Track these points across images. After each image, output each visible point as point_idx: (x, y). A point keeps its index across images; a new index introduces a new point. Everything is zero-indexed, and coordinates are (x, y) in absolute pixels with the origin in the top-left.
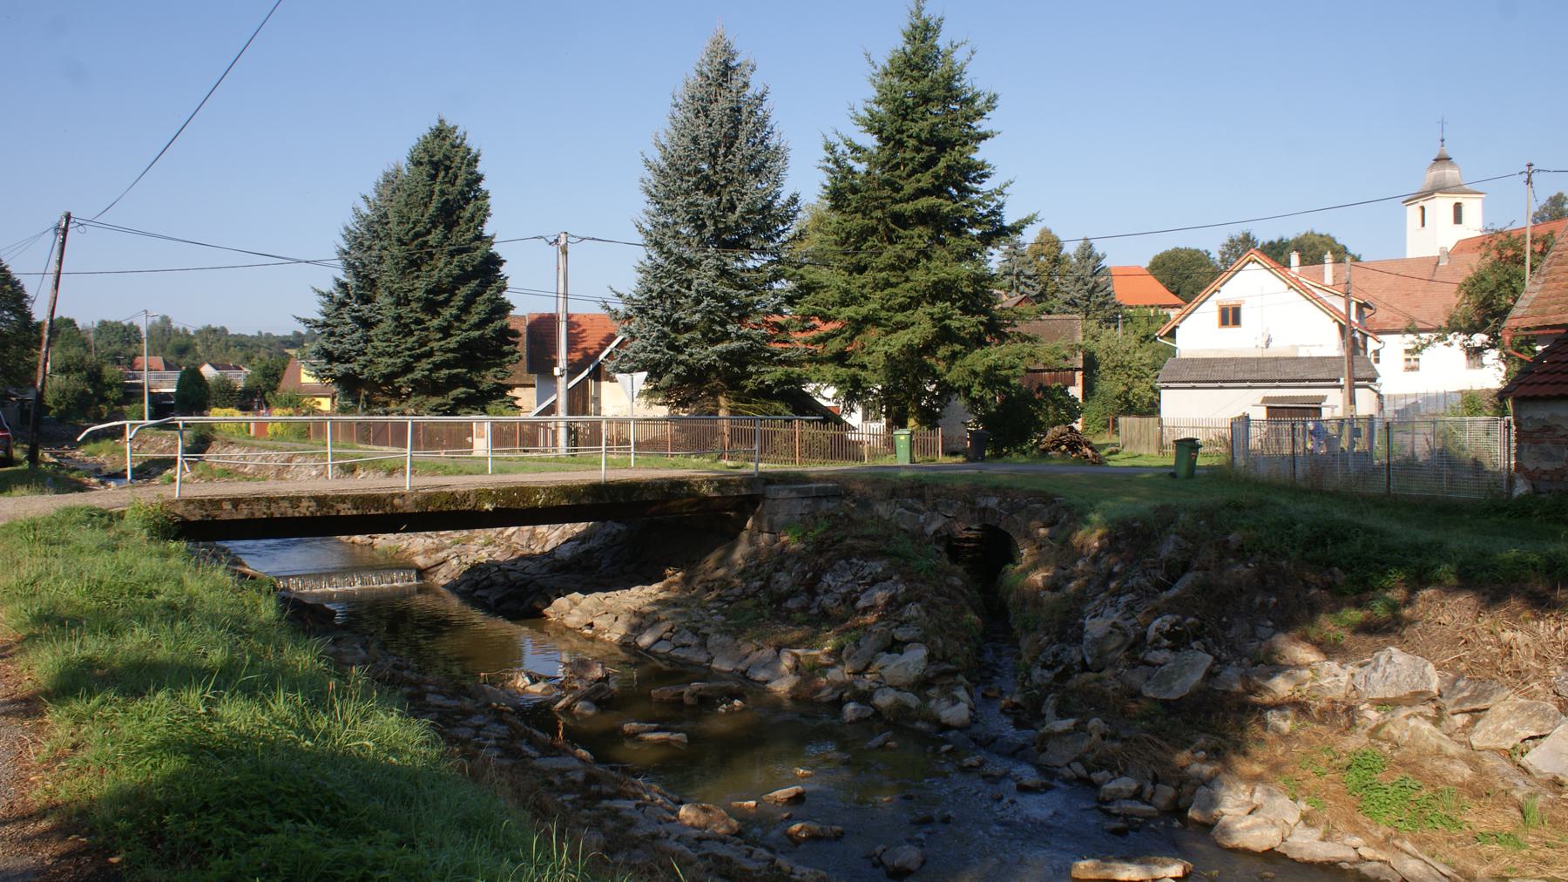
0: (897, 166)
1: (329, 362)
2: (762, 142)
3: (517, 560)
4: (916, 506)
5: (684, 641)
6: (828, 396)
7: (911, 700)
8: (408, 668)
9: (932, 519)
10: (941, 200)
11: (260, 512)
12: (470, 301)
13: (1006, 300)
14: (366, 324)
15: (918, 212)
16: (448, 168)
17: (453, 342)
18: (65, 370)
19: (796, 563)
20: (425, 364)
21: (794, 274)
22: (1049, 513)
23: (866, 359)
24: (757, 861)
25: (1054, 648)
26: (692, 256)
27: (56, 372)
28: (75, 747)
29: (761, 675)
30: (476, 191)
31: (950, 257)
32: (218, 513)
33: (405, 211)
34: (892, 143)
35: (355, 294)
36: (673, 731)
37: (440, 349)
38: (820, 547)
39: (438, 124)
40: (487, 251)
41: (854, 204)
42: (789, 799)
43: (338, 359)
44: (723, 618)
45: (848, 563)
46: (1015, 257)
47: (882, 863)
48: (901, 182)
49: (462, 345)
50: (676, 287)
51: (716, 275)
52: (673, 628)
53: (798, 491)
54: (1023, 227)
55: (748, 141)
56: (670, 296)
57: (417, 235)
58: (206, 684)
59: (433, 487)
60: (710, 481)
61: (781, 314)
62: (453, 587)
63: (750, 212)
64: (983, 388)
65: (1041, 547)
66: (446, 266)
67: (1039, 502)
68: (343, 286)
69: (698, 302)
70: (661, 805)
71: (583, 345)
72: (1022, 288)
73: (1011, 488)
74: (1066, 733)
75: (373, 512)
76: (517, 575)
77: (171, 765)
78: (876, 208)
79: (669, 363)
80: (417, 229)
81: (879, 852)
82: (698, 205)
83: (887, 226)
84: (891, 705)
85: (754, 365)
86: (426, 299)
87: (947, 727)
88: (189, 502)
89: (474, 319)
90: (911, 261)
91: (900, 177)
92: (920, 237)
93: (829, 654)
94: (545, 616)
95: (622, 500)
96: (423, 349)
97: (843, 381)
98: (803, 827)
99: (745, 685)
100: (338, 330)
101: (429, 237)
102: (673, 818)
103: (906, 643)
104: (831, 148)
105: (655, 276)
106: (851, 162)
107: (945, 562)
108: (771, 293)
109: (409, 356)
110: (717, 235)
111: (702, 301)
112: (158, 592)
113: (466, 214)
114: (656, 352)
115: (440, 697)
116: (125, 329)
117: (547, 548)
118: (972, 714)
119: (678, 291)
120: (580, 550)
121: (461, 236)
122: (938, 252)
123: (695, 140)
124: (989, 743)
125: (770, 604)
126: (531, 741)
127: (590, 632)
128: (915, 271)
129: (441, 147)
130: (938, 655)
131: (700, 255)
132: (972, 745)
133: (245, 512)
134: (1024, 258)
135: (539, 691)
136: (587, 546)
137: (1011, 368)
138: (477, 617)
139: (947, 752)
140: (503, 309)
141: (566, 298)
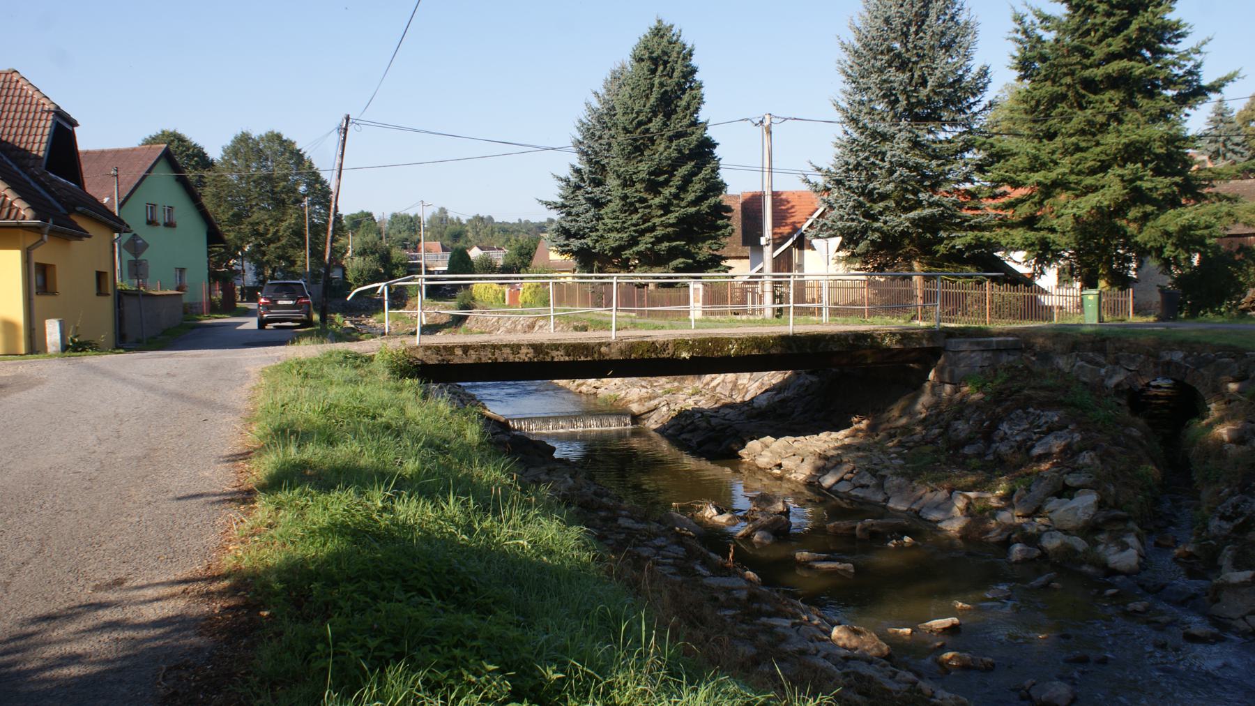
0: (1087, 33)
1: (567, 239)
2: (952, 18)
3: (719, 408)
4: (1098, 359)
5: (863, 482)
6: (1018, 261)
7: (1079, 544)
8: (607, 496)
9: (1114, 372)
10: (1132, 63)
11: (486, 357)
12: (687, 180)
13: (1199, 157)
14: (598, 204)
15: (1109, 76)
16: (666, 63)
17: (672, 218)
18: (362, 253)
19: (974, 412)
20: (648, 238)
21: (984, 143)
22: (1240, 368)
23: (1055, 223)
24: (898, 682)
25: (1234, 499)
26: (886, 130)
27: (356, 255)
28: (270, 526)
29: (934, 516)
30: (691, 82)
31: (1142, 120)
32: (452, 357)
33: (629, 103)
34: (1082, 9)
35: (588, 178)
36: (841, 561)
37: (662, 224)
38: (998, 398)
39: (656, 24)
40: (702, 135)
41: (1044, 73)
42: (945, 629)
43: (575, 236)
44: (902, 462)
45: (1025, 413)
46: (1222, 125)
47: (1030, 698)
48: (1092, 48)
49: (681, 221)
50: (872, 160)
51: (909, 147)
52: (854, 469)
53: (978, 344)
54: (1223, 85)
55: (938, 19)
56: (866, 168)
57: (640, 124)
58: (388, 484)
59: (636, 337)
60: (893, 334)
61: (972, 182)
62: (662, 431)
63: (941, 85)
64: (1177, 249)
65: (1230, 402)
66: (665, 150)
67: (1229, 356)
68: (578, 171)
69: (891, 172)
70: (817, 626)
71: (792, 220)
72: (1229, 155)
73: (1199, 342)
74: (1243, 584)
75: (583, 358)
76: (717, 420)
77: (334, 544)
78: (1065, 75)
79: (864, 231)
80: (640, 118)
81: (1027, 687)
82: (891, 82)
83: (1077, 92)
84: (1057, 548)
85: (945, 230)
86: (649, 180)
87: (1114, 572)
88: (427, 348)
89: (691, 197)
90: (1102, 125)
91: (1090, 43)
92: (1111, 100)
93: (1001, 498)
94: (740, 457)
95: (809, 350)
96: (646, 225)
97: (1032, 244)
98: (954, 656)
99: (918, 525)
100: (574, 211)
101: (650, 125)
102: (826, 637)
103: (1076, 489)
104: (1019, 19)
105: (851, 150)
106: (1040, 32)
107: (1126, 414)
108: (961, 162)
109: (635, 231)
110: (910, 108)
111: (895, 172)
112: (381, 416)
113: (683, 103)
114: (853, 220)
115: (630, 521)
116: (411, 219)
117: (747, 398)
118: (1141, 560)
119: (873, 163)
120: (776, 399)
121: (679, 123)
122: (1130, 115)
123: (887, 21)
124: (1157, 590)
125: (947, 450)
126: (706, 562)
127: (778, 472)
128: (1106, 135)
129: (659, 44)
130: (1110, 502)
131: (893, 129)
132: (1139, 591)
133: (474, 357)
134: (1232, 125)
135: (724, 521)
136: (782, 396)
137: (1207, 227)
138: (690, 462)
139: (1113, 596)
140: (717, 187)
141: (771, 171)
